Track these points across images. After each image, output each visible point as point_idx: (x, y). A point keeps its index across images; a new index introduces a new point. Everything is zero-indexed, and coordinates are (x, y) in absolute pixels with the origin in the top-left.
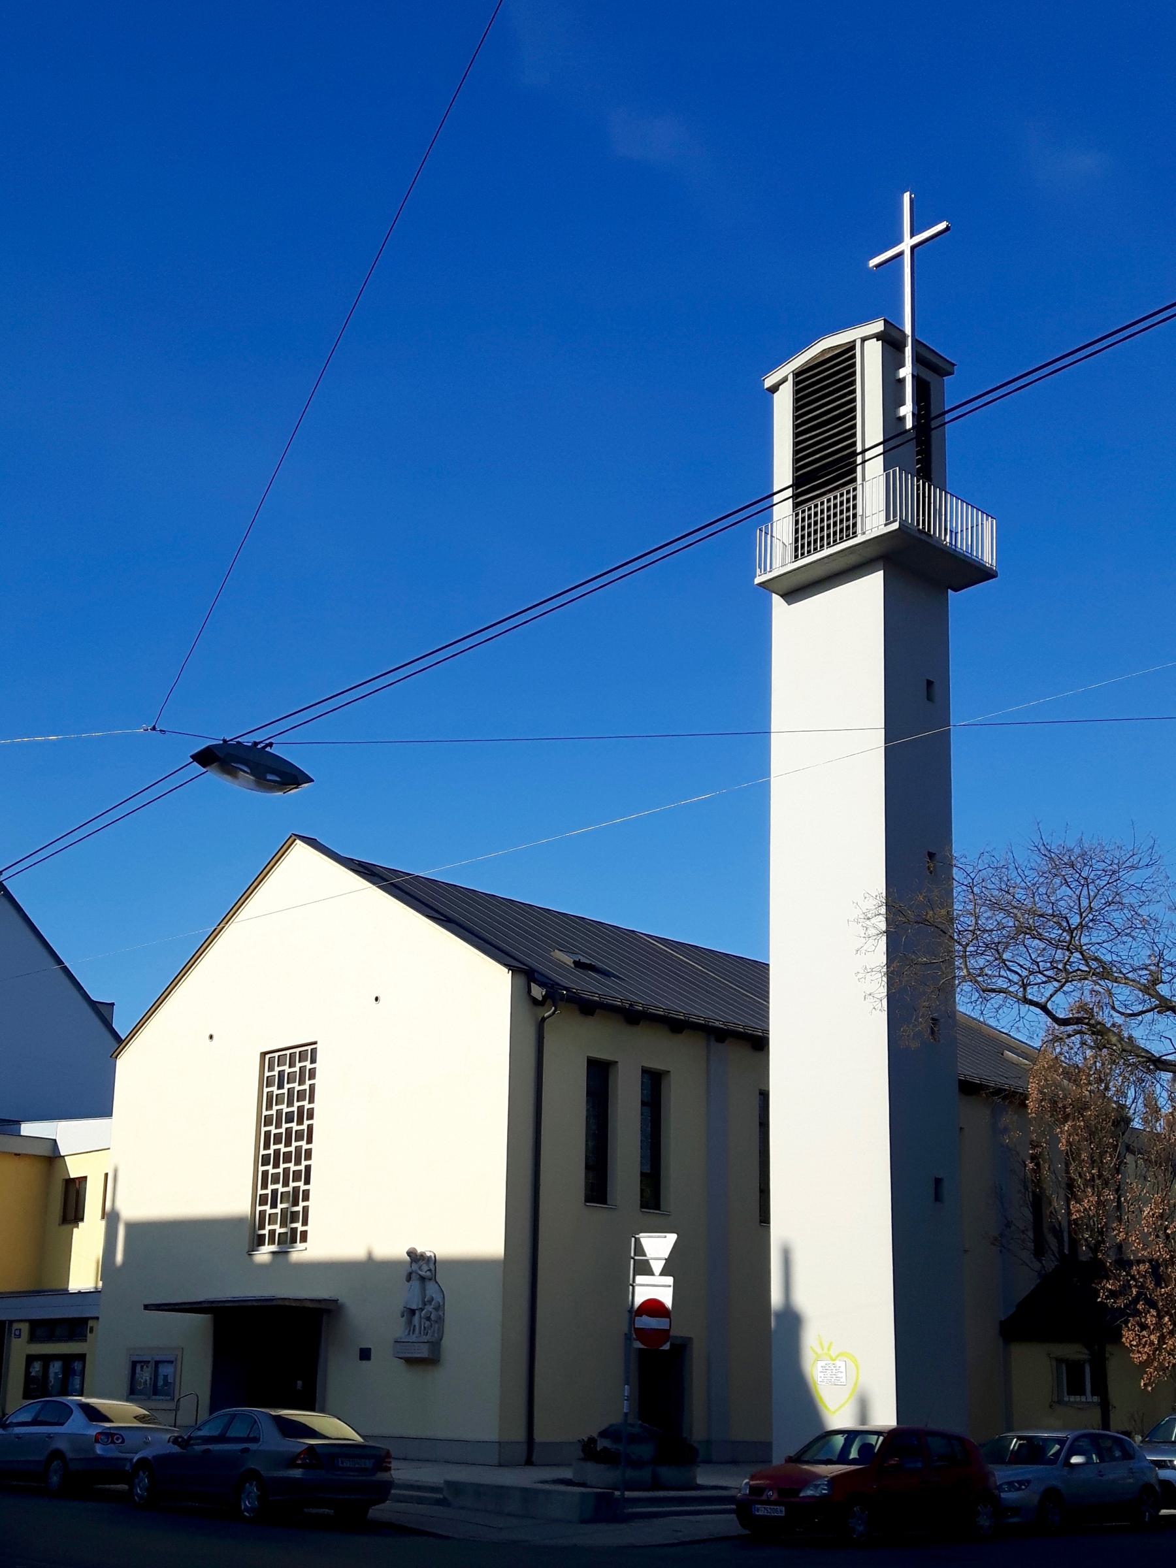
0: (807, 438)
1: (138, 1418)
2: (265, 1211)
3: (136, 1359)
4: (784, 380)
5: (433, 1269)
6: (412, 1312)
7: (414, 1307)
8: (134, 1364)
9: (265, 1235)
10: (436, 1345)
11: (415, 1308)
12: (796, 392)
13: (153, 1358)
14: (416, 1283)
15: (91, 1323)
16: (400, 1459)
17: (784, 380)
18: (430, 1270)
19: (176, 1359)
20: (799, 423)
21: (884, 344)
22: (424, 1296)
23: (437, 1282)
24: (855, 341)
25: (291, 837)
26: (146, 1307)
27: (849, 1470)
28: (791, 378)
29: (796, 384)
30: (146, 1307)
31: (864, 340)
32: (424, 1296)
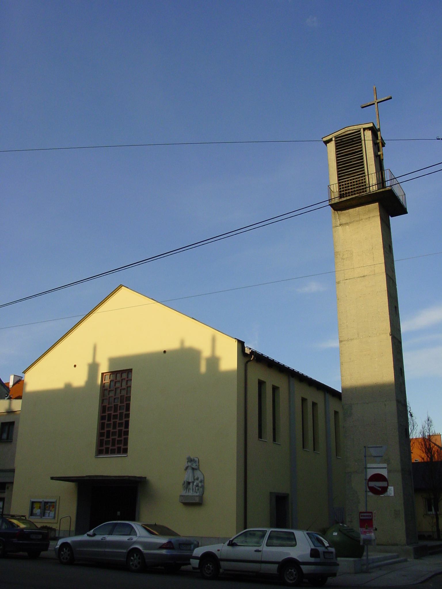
0: (359, 151)
1: (162, 547)
2: (115, 439)
3: (33, 500)
4: (331, 140)
5: (198, 465)
6: (189, 483)
7: (190, 481)
8: (33, 503)
9: (103, 449)
10: (201, 497)
11: (191, 481)
12: (336, 144)
13: (43, 501)
14: (190, 471)
15: (7, 485)
16: (39, 522)
17: (331, 140)
18: (197, 465)
19: (56, 501)
20: (338, 154)
21: (8, 386)
22: (194, 477)
23: (200, 471)
24: (361, 129)
25: (120, 285)
26: (52, 478)
27: (131, 522)
28: (333, 139)
29: (336, 141)
30: (52, 478)
31: (364, 129)
32: (194, 477)
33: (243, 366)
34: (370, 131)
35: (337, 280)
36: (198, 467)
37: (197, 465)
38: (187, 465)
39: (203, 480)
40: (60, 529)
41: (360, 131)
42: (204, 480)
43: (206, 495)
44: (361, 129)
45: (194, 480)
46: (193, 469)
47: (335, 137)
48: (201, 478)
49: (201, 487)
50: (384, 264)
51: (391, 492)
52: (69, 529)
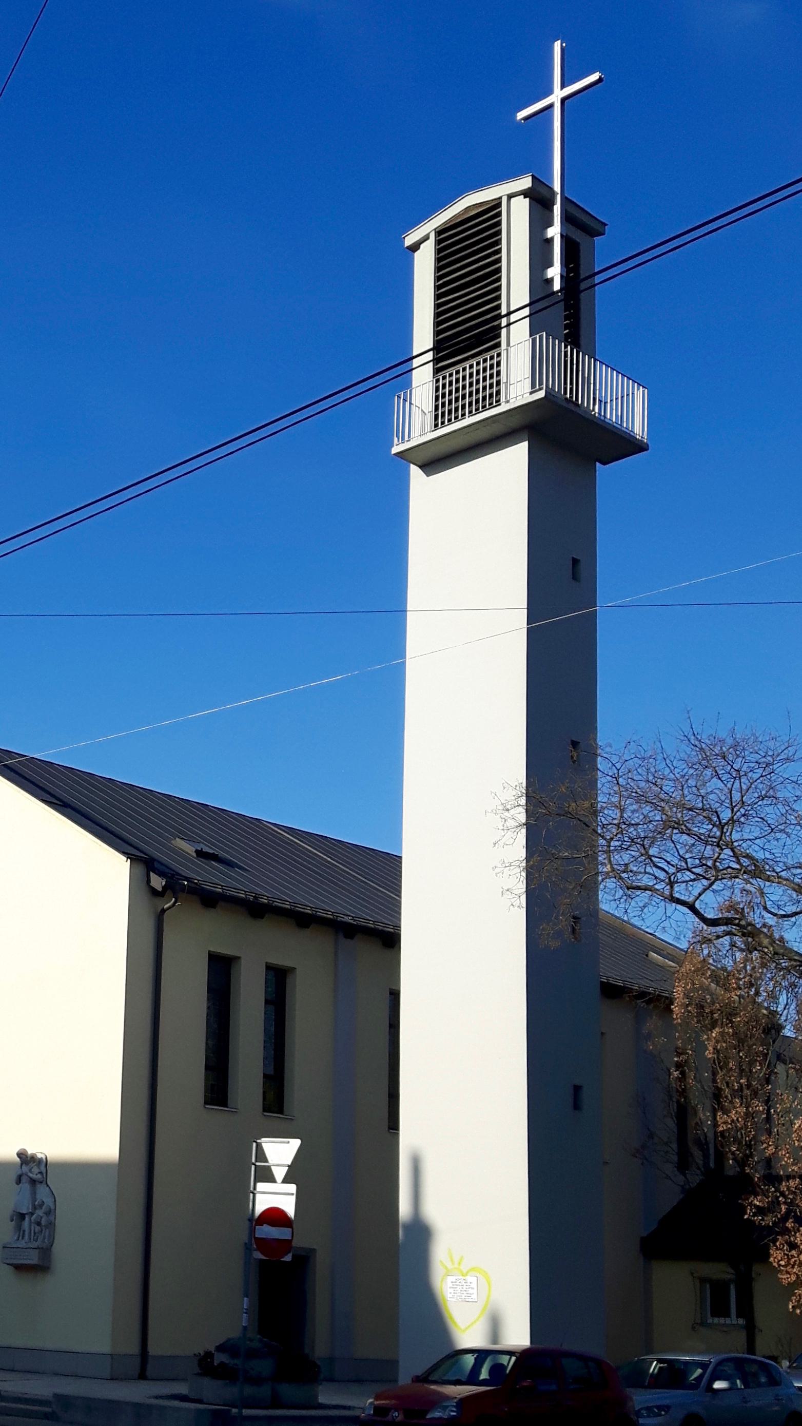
4: (426, 238)
5: (44, 1171)
6: (22, 1216)
10: (46, 1252)
12: (438, 251)
14: (26, 1186)
17: (426, 238)
18: (41, 1173)
22: (34, 1199)
23: (48, 1186)
31: (510, 197)
32: (34, 1199)
33: (149, 925)
34: (528, 199)
35: (164, 883)
36: (45, 1175)
37: (41, 1173)
38: (20, 1173)
39: (52, 1207)
40: (153, 1350)
41: (499, 205)
42: (55, 1209)
43: (58, 1249)
44: (503, 198)
45: (35, 1208)
46: (33, 1182)
47: (435, 229)
48: (48, 1201)
49: (46, 1227)
50: (526, 611)
51: (471, 1291)
52: (134, 1348)
